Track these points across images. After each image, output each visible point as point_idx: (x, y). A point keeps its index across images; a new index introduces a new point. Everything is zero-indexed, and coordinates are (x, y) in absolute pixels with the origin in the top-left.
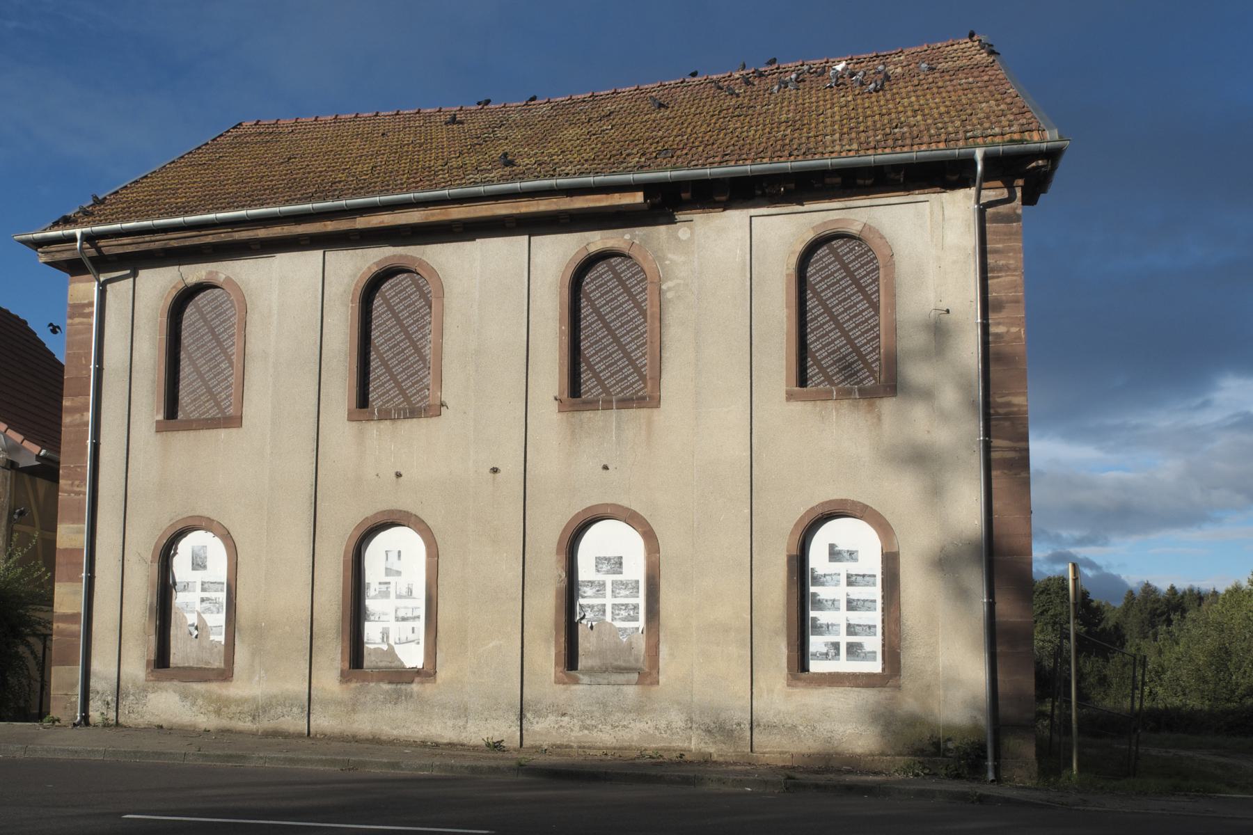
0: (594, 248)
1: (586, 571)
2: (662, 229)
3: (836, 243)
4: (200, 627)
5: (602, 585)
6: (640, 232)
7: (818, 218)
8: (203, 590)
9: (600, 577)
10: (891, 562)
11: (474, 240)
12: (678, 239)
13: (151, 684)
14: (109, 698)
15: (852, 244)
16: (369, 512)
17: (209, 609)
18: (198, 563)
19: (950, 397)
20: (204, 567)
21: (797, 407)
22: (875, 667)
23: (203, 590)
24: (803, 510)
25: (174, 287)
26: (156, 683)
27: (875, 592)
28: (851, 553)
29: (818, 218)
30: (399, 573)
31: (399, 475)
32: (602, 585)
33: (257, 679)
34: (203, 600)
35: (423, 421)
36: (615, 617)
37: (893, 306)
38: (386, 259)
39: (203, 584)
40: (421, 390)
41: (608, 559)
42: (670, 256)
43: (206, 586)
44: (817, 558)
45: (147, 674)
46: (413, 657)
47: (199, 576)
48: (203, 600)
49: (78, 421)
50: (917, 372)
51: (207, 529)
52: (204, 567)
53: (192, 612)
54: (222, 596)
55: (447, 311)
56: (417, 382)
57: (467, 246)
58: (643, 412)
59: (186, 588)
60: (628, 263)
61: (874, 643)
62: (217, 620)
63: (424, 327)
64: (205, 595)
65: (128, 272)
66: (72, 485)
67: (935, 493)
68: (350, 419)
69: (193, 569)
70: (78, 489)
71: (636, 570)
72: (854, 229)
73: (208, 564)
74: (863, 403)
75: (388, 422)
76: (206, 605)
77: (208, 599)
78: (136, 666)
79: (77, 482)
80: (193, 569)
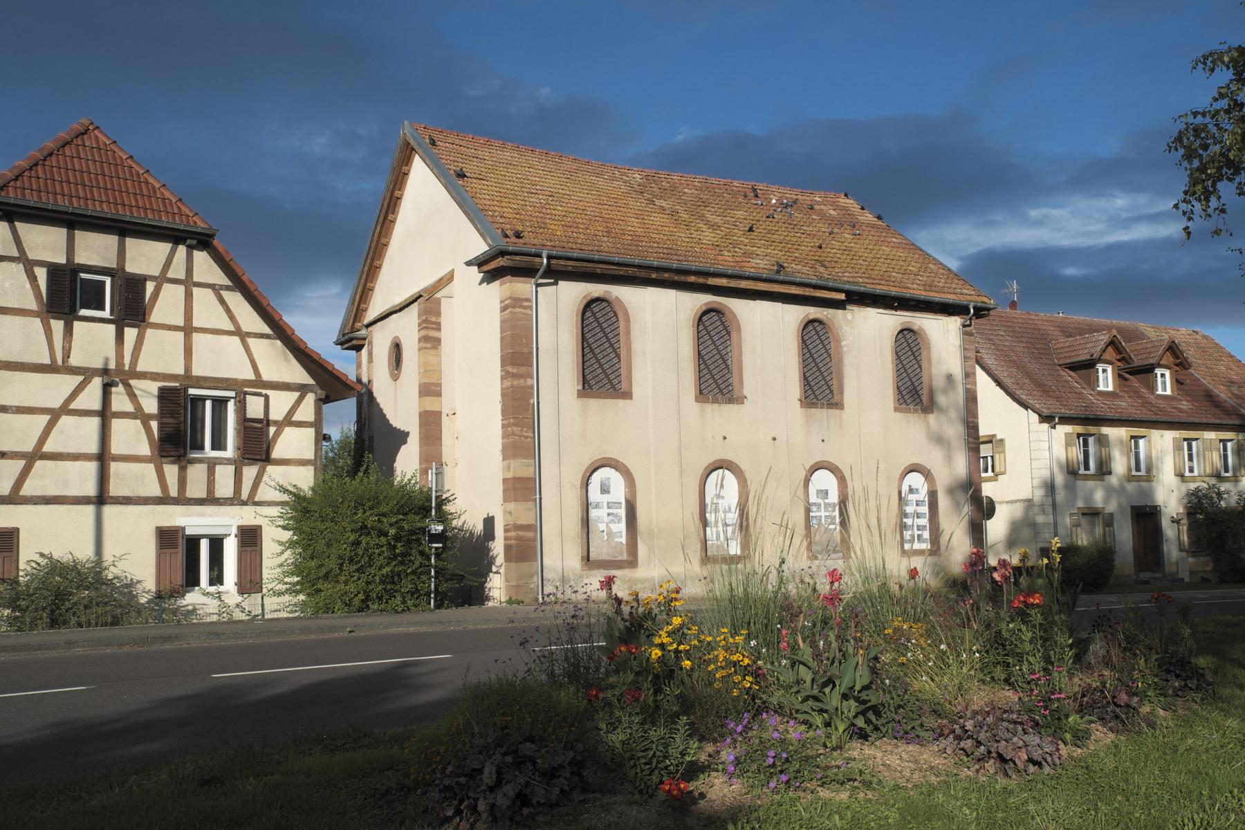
0: (596, 295)
1: (813, 498)
2: (840, 311)
3: (816, 324)
4: (611, 534)
5: (820, 505)
6: (831, 311)
7: (902, 319)
8: (609, 507)
9: (819, 501)
10: (933, 495)
11: (755, 300)
12: (847, 318)
13: (585, 572)
14: (558, 584)
15: (911, 334)
16: (711, 460)
17: (613, 520)
18: (605, 490)
19: (953, 414)
20: (609, 492)
21: (898, 415)
22: (925, 546)
23: (609, 507)
24: (903, 468)
25: (584, 297)
26: (589, 572)
27: (925, 509)
28: (917, 490)
29: (902, 319)
30: (723, 497)
31: (725, 438)
32: (820, 505)
33: (653, 565)
34: (609, 514)
35: (735, 406)
36: (909, 521)
37: (930, 368)
38: (710, 303)
39: (608, 503)
40: (728, 386)
41: (822, 491)
42: (844, 327)
43: (610, 505)
44: (594, 494)
45: (582, 566)
46: (735, 549)
47: (605, 499)
48: (609, 514)
49: (523, 385)
50: (941, 399)
51: (611, 467)
52: (609, 492)
53: (602, 522)
54: (622, 512)
55: (743, 341)
56: (725, 381)
57: (751, 303)
58: (837, 411)
59: (597, 506)
60: (822, 326)
61: (926, 535)
62: (621, 527)
63: (727, 347)
64: (610, 511)
65: (553, 281)
66: (522, 430)
67: (949, 459)
68: (896, 410)
69: (602, 493)
70: (526, 434)
71: (834, 497)
72: (915, 328)
73: (611, 490)
74: (922, 415)
75: (717, 405)
76: (611, 517)
77: (612, 514)
78: (573, 561)
79: (525, 429)
80: (602, 493)
